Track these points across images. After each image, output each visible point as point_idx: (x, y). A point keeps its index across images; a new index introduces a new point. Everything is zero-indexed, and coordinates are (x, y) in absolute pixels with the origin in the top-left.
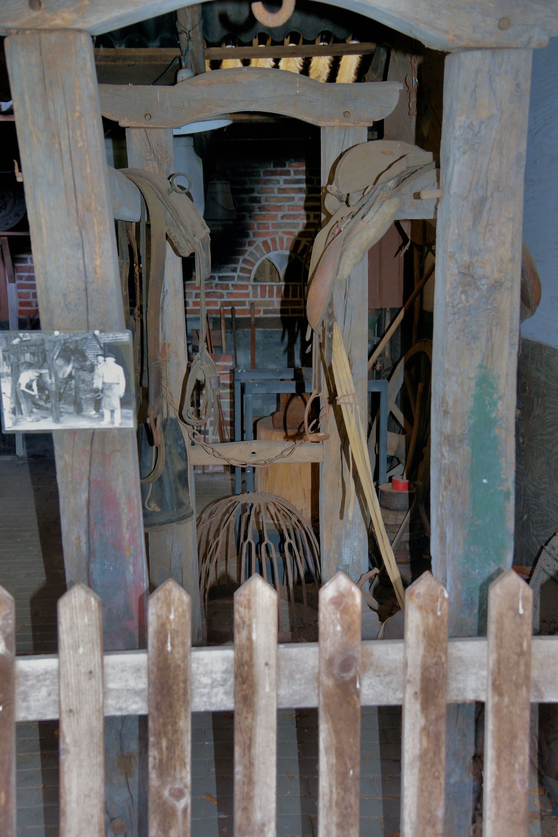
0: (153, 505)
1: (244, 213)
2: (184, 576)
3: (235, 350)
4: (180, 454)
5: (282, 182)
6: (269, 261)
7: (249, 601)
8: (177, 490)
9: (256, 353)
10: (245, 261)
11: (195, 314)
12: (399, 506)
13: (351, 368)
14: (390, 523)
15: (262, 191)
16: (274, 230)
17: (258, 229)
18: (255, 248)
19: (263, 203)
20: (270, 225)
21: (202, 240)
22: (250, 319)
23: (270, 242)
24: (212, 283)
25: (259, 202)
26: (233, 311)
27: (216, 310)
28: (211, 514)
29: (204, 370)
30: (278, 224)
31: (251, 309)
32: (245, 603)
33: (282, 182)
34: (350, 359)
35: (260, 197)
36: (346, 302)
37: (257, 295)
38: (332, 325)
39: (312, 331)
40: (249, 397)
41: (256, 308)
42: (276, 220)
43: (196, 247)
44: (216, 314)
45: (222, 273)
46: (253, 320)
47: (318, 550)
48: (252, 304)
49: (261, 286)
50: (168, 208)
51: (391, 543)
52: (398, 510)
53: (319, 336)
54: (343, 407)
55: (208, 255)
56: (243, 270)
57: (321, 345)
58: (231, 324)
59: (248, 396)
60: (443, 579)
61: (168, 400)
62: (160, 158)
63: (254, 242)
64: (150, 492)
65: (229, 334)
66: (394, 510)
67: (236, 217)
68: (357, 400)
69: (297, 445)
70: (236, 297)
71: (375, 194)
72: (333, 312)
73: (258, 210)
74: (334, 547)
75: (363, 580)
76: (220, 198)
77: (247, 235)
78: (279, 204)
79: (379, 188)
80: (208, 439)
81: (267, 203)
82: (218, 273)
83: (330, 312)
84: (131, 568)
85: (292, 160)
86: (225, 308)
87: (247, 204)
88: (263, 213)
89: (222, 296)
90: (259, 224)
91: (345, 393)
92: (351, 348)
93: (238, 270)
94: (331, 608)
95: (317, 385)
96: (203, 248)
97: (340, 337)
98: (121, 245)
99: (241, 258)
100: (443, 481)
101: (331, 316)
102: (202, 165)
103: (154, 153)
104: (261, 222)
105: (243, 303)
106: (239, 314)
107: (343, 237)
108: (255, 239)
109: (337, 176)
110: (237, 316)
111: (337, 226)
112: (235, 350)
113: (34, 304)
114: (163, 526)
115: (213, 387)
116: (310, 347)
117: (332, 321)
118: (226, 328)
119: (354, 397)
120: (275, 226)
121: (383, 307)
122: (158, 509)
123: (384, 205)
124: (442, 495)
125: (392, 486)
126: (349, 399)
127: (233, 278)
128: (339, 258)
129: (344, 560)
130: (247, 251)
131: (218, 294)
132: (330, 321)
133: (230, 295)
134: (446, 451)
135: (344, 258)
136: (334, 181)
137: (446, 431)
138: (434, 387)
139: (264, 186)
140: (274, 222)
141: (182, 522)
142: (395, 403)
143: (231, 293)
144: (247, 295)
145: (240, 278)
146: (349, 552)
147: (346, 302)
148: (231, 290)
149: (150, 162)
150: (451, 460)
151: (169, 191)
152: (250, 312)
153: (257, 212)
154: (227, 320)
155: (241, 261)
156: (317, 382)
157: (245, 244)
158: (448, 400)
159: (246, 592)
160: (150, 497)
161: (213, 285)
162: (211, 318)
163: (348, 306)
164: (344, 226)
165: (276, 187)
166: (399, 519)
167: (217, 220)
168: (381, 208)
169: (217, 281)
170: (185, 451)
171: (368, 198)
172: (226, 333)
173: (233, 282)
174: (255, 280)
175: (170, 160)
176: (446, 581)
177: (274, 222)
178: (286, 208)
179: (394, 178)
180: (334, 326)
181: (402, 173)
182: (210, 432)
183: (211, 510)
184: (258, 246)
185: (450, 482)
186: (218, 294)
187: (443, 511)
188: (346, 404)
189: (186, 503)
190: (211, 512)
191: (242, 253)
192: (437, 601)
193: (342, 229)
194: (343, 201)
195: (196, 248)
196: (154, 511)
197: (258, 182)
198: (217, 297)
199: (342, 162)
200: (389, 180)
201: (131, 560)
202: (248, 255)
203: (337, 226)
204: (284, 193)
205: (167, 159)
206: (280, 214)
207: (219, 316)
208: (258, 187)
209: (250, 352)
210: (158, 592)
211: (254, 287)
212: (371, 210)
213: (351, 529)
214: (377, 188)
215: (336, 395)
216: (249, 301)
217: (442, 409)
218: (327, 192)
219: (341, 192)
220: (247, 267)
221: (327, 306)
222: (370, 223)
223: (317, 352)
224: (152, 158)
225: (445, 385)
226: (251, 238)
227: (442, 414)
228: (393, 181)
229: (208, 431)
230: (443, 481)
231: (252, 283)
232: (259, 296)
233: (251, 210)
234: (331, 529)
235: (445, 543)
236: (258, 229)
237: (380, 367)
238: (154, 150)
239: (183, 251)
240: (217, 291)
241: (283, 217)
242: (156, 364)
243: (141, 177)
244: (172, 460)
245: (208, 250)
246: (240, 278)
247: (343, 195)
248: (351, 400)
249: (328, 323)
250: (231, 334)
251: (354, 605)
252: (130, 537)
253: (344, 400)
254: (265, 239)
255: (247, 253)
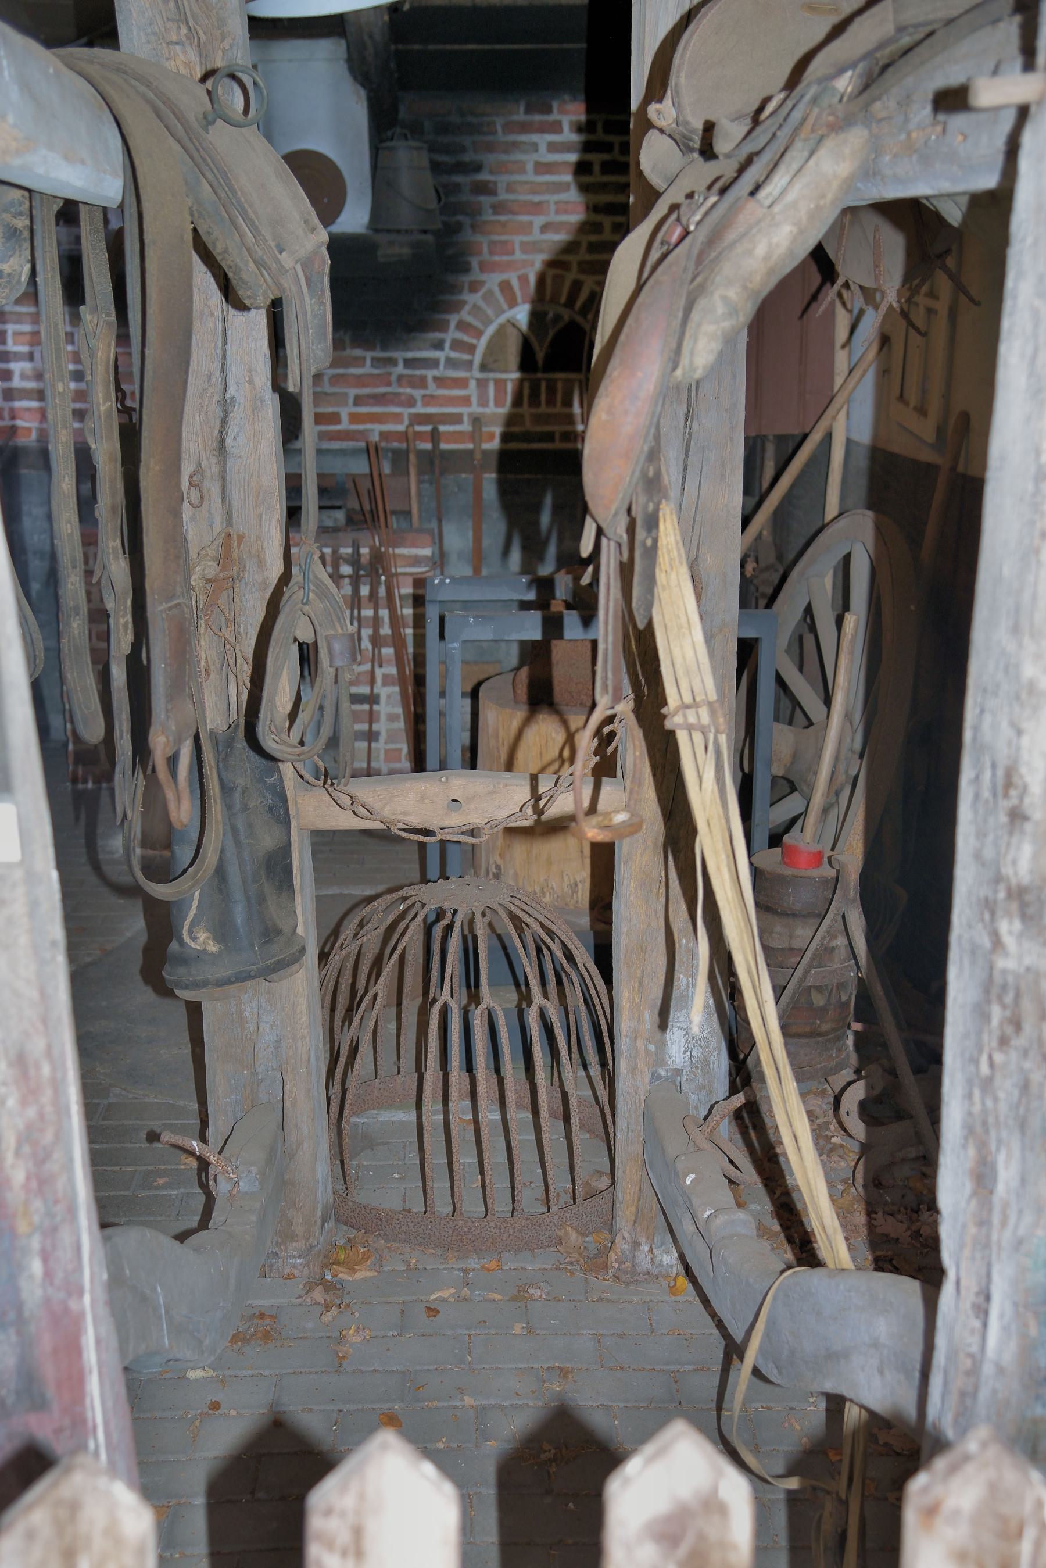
0: (202, 936)
1: (460, 218)
2: (287, 1088)
3: (440, 520)
4: (271, 808)
5: (543, 148)
6: (514, 325)
7: (358, 1532)
8: (262, 899)
9: (484, 526)
10: (462, 326)
11: (353, 440)
12: (798, 907)
13: (699, 596)
14: (775, 944)
15: (501, 168)
16: (524, 257)
17: (491, 253)
18: (485, 298)
19: (503, 196)
20: (517, 247)
21: (307, 264)
22: (470, 453)
23: (515, 283)
24: (390, 374)
25: (494, 193)
26: (435, 436)
27: (398, 432)
28: (361, 925)
29: (313, 616)
30: (534, 243)
31: (474, 431)
32: (344, 1537)
33: (543, 148)
34: (697, 579)
35: (495, 183)
36: (690, 433)
37: (488, 402)
38: (657, 510)
39: (600, 532)
40: (454, 648)
41: (485, 429)
42: (530, 233)
43: (287, 283)
44: (400, 442)
45: (411, 350)
46: (478, 456)
47: (608, 1012)
48: (476, 420)
49: (497, 382)
50: (205, 168)
51: (779, 991)
52: (794, 915)
53: (620, 545)
54: (682, 737)
55: (323, 304)
56: (456, 345)
57: (626, 571)
58: (432, 463)
59: (450, 645)
60: (978, 1294)
61: (239, 676)
62: (203, 37)
63: (482, 283)
64: (195, 904)
65: (426, 486)
66: (785, 914)
67: (440, 226)
68: (721, 720)
69: (562, 789)
70: (441, 405)
71: (797, 115)
72: (658, 474)
73: (490, 211)
74: (648, 1026)
75: (715, 1117)
76: (405, 182)
77: (466, 269)
78: (537, 198)
79: (808, 97)
80: (379, 712)
81: (511, 197)
82: (403, 350)
83: (651, 474)
84: (36, 1267)
85: (567, 97)
86: (418, 428)
87: (465, 197)
88: (502, 218)
89: (411, 402)
90: (492, 243)
91: (688, 699)
92: (698, 549)
93: (447, 345)
94: (648, 1552)
95: (610, 683)
96: (309, 286)
97: (677, 543)
98: (90, 274)
99: (453, 319)
100: (995, 1021)
101: (653, 485)
102: (365, 104)
103: (187, 23)
104: (496, 238)
105: (457, 419)
106: (448, 442)
107: (696, 251)
108: (484, 277)
109: (678, 77)
110: (444, 446)
111: (678, 220)
112: (440, 520)
113: (6, 415)
114: (226, 987)
115: (339, 663)
116: (590, 569)
117: (656, 499)
118: (420, 473)
119: (713, 713)
120: (526, 247)
121: (764, 433)
122: (213, 948)
123: (822, 152)
124: (990, 1057)
125: (783, 858)
126: (697, 713)
127: (434, 363)
128: (680, 314)
129: (670, 1057)
130: (465, 303)
131: (403, 398)
132: (650, 499)
133: (429, 399)
134: (1010, 933)
135: (695, 316)
136: (669, 92)
137: (1016, 873)
138: (976, 729)
139: (504, 157)
140: (525, 238)
141: (274, 976)
142: (787, 652)
143: (432, 396)
144: (466, 401)
145: (451, 363)
146: (683, 1040)
147: (690, 433)
148: (432, 389)
149: (178, 48)
150: (1028, 961)
151: (205, 117)
152: (472, 436)
153: (488, 216)
154: (421, 453)
155: (453, 325)
156: (610, 675)
157: (463, 288)
158: (1028, 779)
159: (348, 1502)
160: (195, 915)
161: (393, 378)
162: (387, 450)
163: (692, 443)
164: (698, 218)
165: (529, 160)
166: (798, 936)
167: (398, 231)
168: (812, 162)
169: (400, 369)
170: (285, 801)
171: (774, 129)
172: (420, 482)
173: (435, 372)
174: (483, 367)
175: (231, 46)
176: (988, 1298)
177: (525, 238)
178: (553, 208)
179: (853, 65)
180: (661, 514)
181: (881, 46)
182: (383, 699)
183: (360, 918)
184: (490, 292)
185: (1018, 1027)
186: (403, 398)
187: (989, 1103)
188: (690, 728)
189: (286, 929)
190: (361, 921)
191: (456, 307)
192: (1020, 1534)
193: (692, 228)
194: (691, 150)
195: (285, 285)
196: (205, 950)
197: (490, 148)
198: (401, 404)
199: (692, 35)
200: (841, 71)
201: (35, 1243)
202: (469, 313)
203: (678, 220)
204: (547, 173)
205: (222, 41)
206: (539, 221)
207: (404, 446)
208: (490, 159)
209: (470, 524)
210: (30, 1508)
211: (482, 384)
212: (782, 168)
213: (688, 987)
214: (802, 97)
215: (664, 703)
216: (470, 415)
217: (1005, 804)
218: (649, 125)
219: (687, 123)
220: (466, 338)
221: (643, 459)
222: (777, 209)
223: (612, 591)
224: (184, 39)
225: (1019, 732)
226: (476, 275)
227: (1004, 819)
228: (849, 73)
229: (378, 696)
230: (995, 1021)
231: (477, 374)
232: (491, 403)
233: (474, 212)
234: (641, 984)
235: (991, 1192)
236: (491, 253)
237: (754, 569)
238: (188, 14)
239: (249, 293)
240: (401, 390)
241: (545, 228)
242: (170, 609)
243: (125, 72)
244: (250, 826)
245: (323, 291)
246: (451, 363)
247: (694, 131)
248: (705, 718)
249: (646, 507)
250: (431, 484)
251: (725, 1545)
252: (28, 1178)
253: (685, 717)
254: (505, 276)
255: (467, 308)
